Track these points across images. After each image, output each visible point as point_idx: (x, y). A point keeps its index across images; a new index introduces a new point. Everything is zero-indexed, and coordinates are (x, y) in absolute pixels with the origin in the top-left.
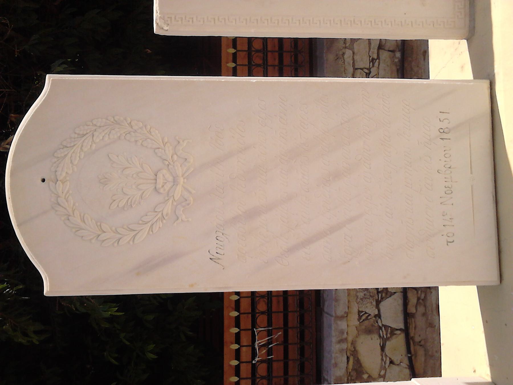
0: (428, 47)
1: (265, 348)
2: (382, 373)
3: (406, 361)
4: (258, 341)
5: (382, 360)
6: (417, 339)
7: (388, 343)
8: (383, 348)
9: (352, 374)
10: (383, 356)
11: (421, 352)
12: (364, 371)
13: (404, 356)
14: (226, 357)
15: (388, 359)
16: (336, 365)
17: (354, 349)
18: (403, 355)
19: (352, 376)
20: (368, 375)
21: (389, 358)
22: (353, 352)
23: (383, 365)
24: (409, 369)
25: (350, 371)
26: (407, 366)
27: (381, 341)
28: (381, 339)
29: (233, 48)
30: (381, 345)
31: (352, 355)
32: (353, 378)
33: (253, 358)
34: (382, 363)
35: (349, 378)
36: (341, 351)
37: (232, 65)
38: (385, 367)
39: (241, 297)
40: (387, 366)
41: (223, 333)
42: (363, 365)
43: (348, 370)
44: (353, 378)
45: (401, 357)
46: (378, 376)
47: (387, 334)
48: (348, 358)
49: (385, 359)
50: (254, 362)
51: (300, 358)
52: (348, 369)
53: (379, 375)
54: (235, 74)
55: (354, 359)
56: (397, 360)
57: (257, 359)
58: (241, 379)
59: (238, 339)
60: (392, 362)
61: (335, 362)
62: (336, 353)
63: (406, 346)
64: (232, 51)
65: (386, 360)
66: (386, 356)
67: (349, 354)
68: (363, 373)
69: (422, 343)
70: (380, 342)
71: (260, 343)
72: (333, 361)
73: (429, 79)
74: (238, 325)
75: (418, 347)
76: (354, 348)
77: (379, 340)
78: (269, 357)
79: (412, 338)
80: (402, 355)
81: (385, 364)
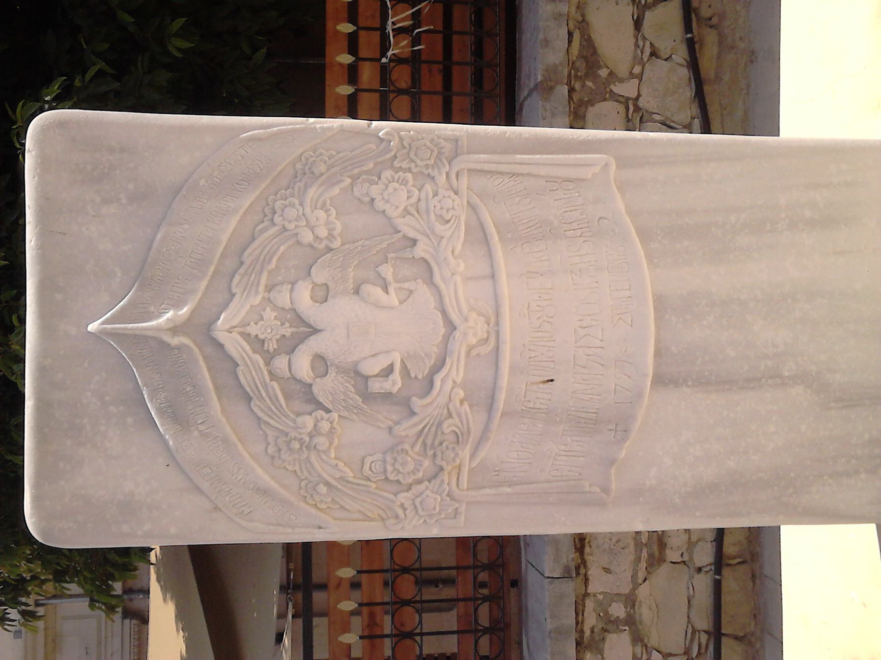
0: (779, 131)
1: (406, 36)
2: (637, 70)
3: (681, 54)
4: (392, 50)
5: (637, 45)
6: (705, 12)
7: (648, 15)
8: (638, 24)
9: (578, 64)
10: (639, 39)
11: (710, 38)
12: (601, 63)
13: (678, 41)
14: (330, 49)
15: (648, 44)
16: (546, 43)
17: (581, 19)
18: (677, 40)
19: (577, 70)
20: (610, 70)
21: (650, 43)
22: (580, 23)
23: (638, 55)
24: (687, 67)
25: (575, 59)
26: (685, 63)
27: (635, 9)
28: (636, 6)
29: (350, 22)
30: (635, 18)
31: (579, 29)
32: (579, 74)
33: (383, 54)
34: (635, 50)
35: (573, 72)
36: (558, 16)
37: (346, 90)
38: (642, 59)
39: (359, 28)
40: (645, 59)
41: (325, 46)
42: (599, 52)
43: (570, 56)
44: (579, 74)
45: (674, 43)
46: (627, 75)
47: (628, 106)
48: (570, 34)
49: (641, 43)
50: (384, 60)
51: (475, 91)
52: (570, 55)
53: (631, 72)
54: (353, 114)
55: (582, 36)
56: (666, 48)
57: (389, 53)
58: (359, 59)
59: (352, 74)
60: (654, 54)
61: (545, 39)
62: (547, 20)
63: (682, 11)
64: (346, 59)
65: (643, 46)
66: (644, 39)
67: (572, 27)
68: (600, 67)
69: (715, 20)
70: (634, 9)
71: (398, 21)
72: (541, 36)
73: (779, 136)
74: (353, 20)
75: (706, 31)
76: (583, 16)
77: (631, 7)
78: (415, 48)
79: (696, 11)
80: (675, 41)
81: (642, 54)
